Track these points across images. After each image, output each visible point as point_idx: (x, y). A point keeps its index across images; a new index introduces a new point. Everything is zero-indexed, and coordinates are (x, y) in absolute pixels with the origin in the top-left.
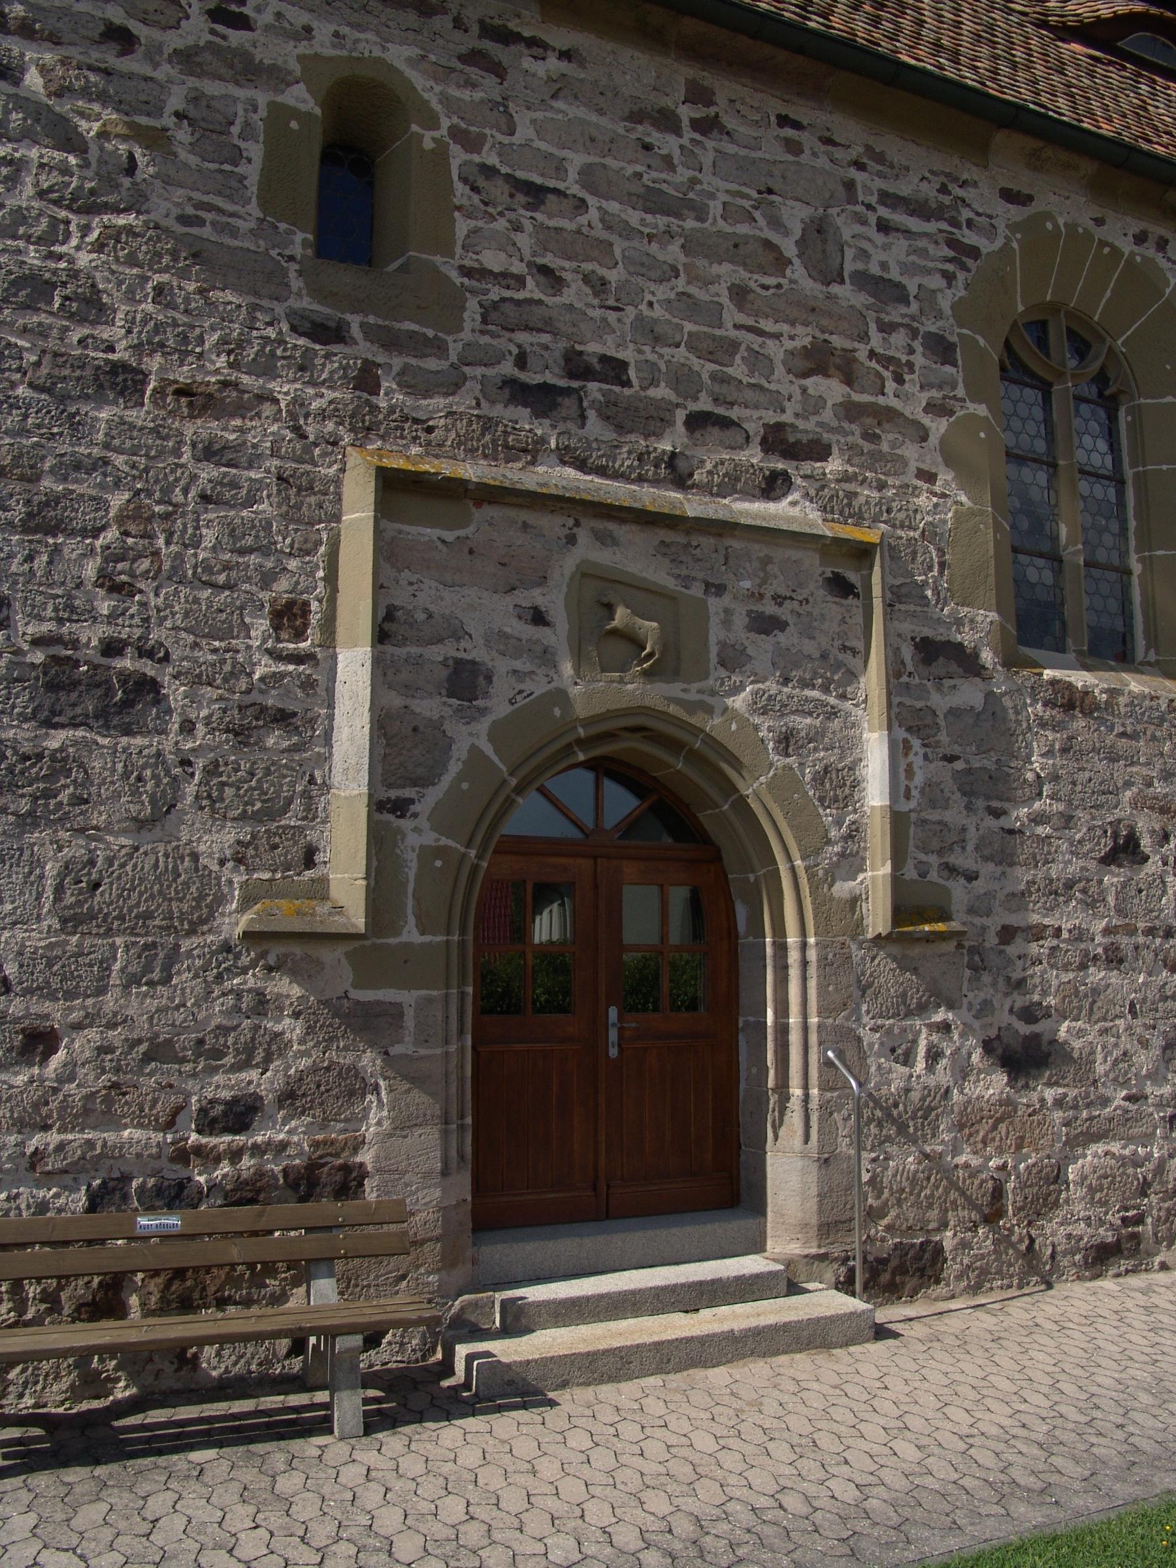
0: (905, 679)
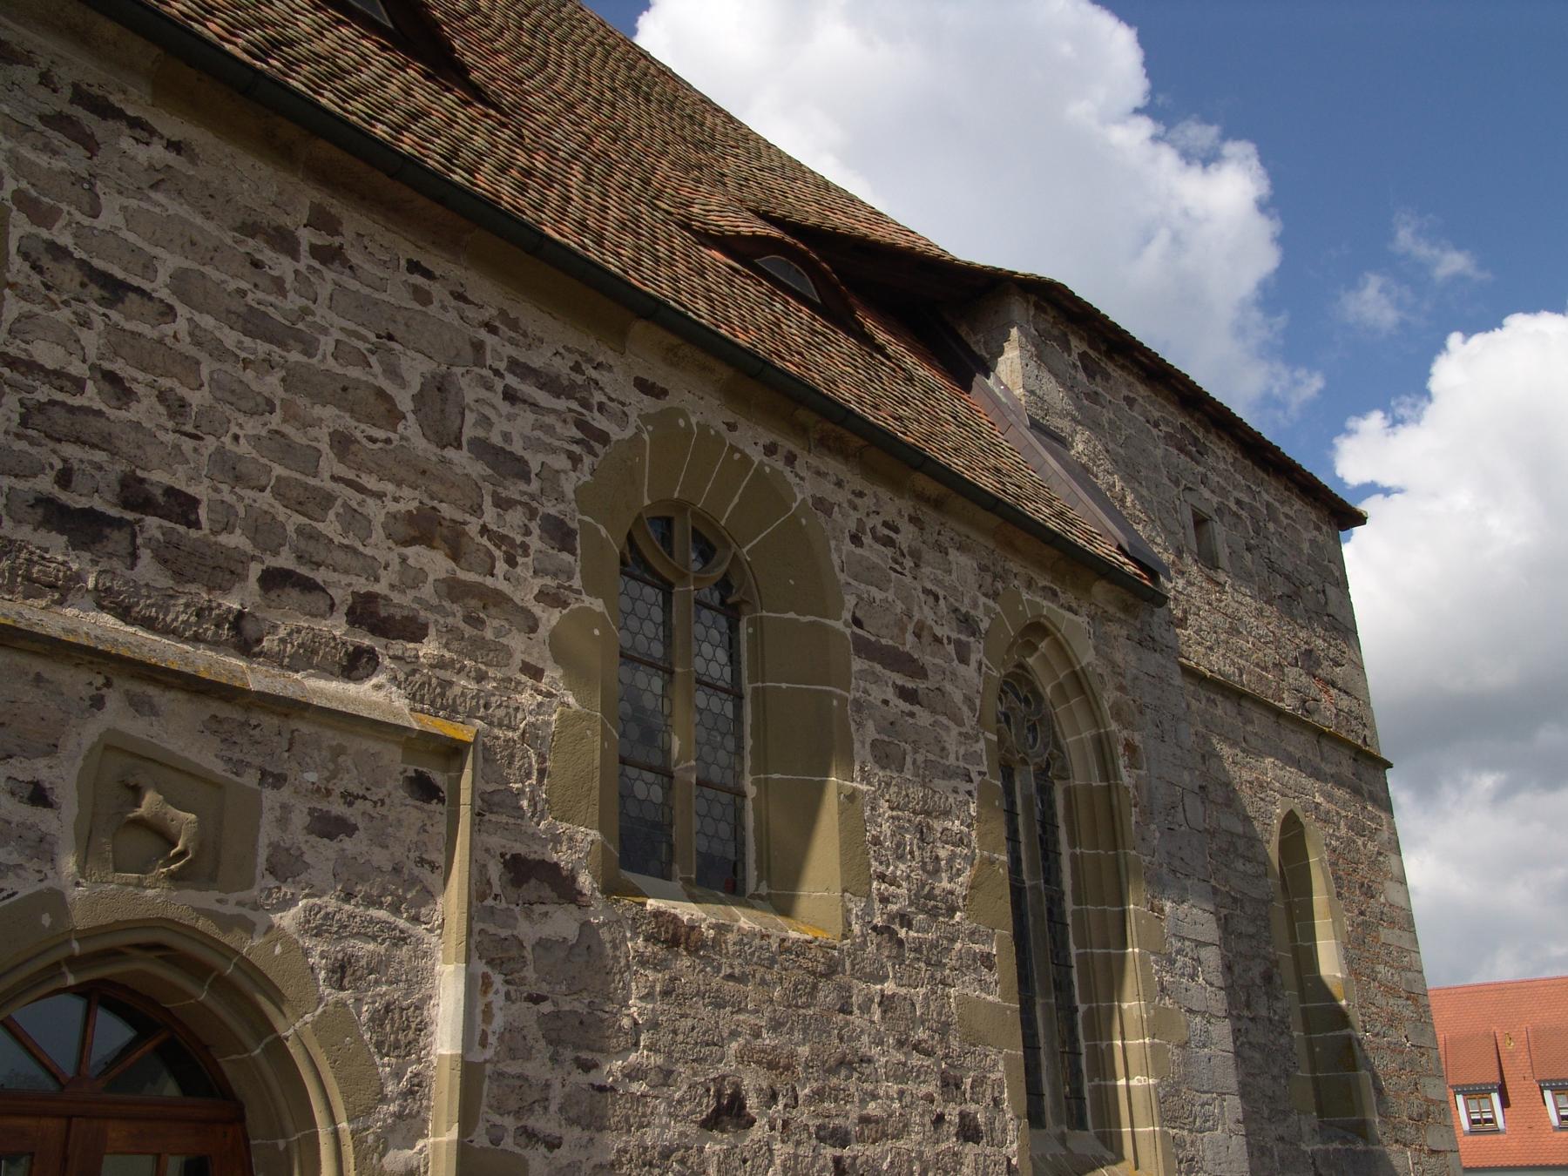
0: (489, 902)
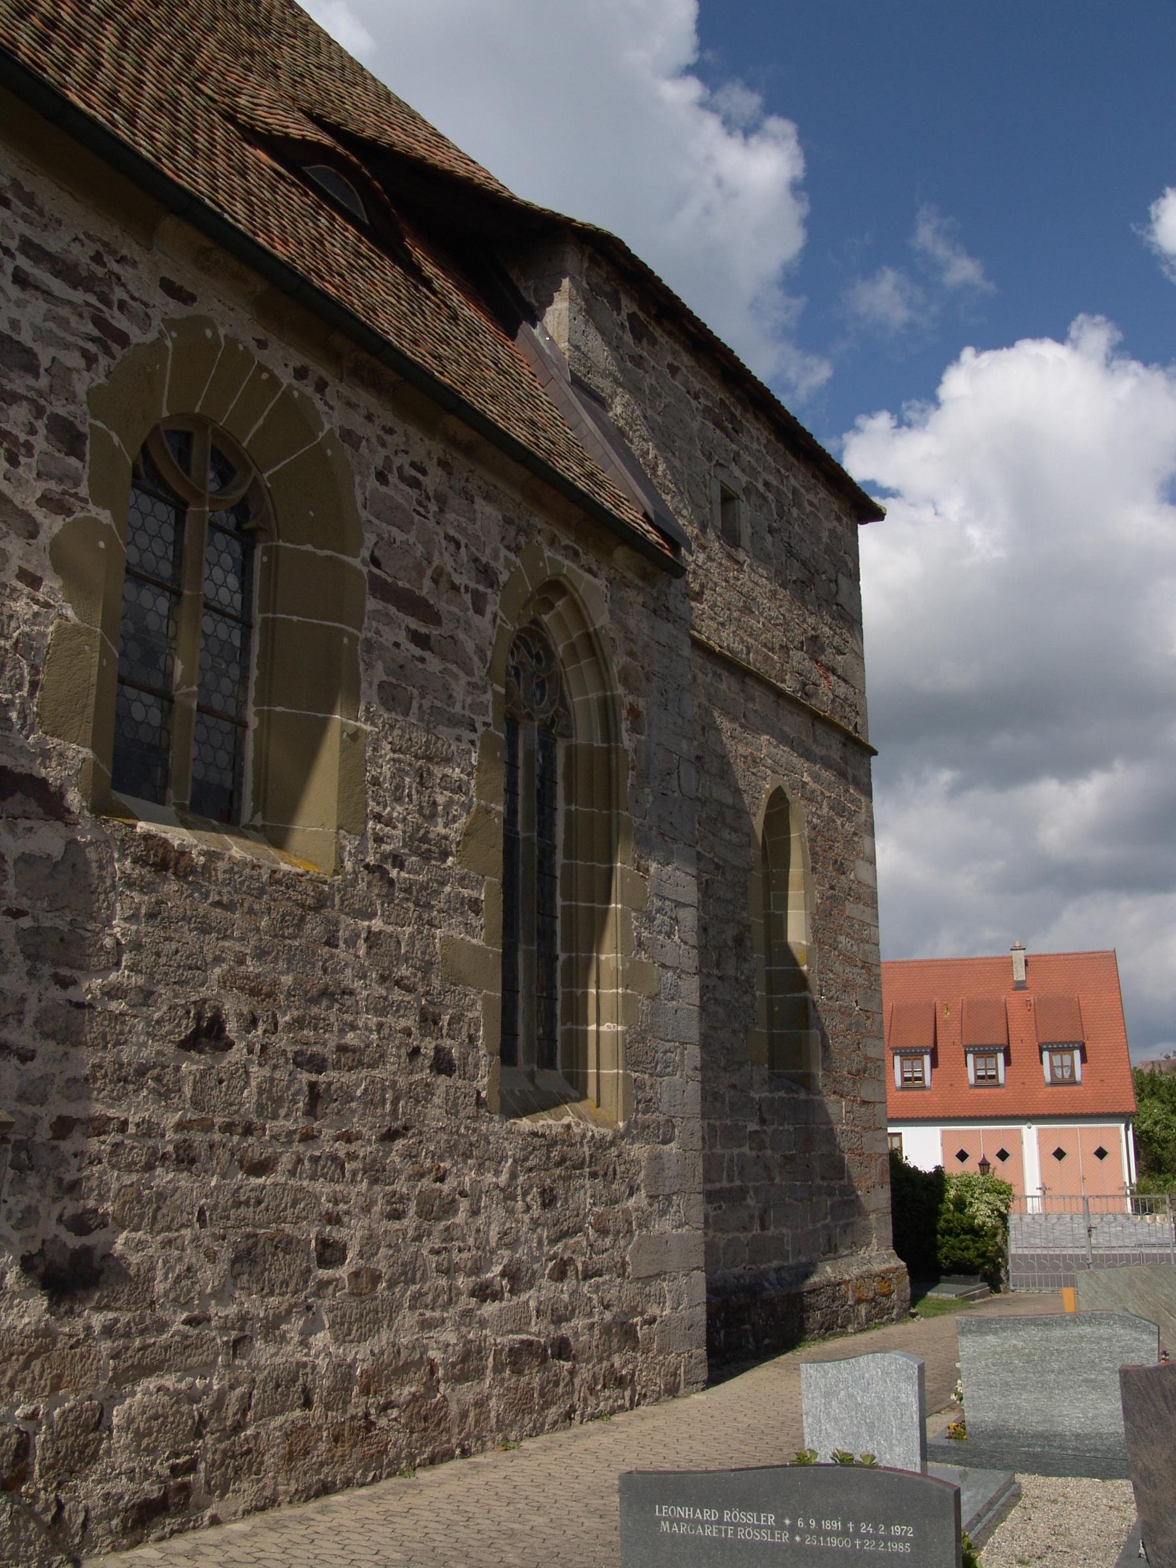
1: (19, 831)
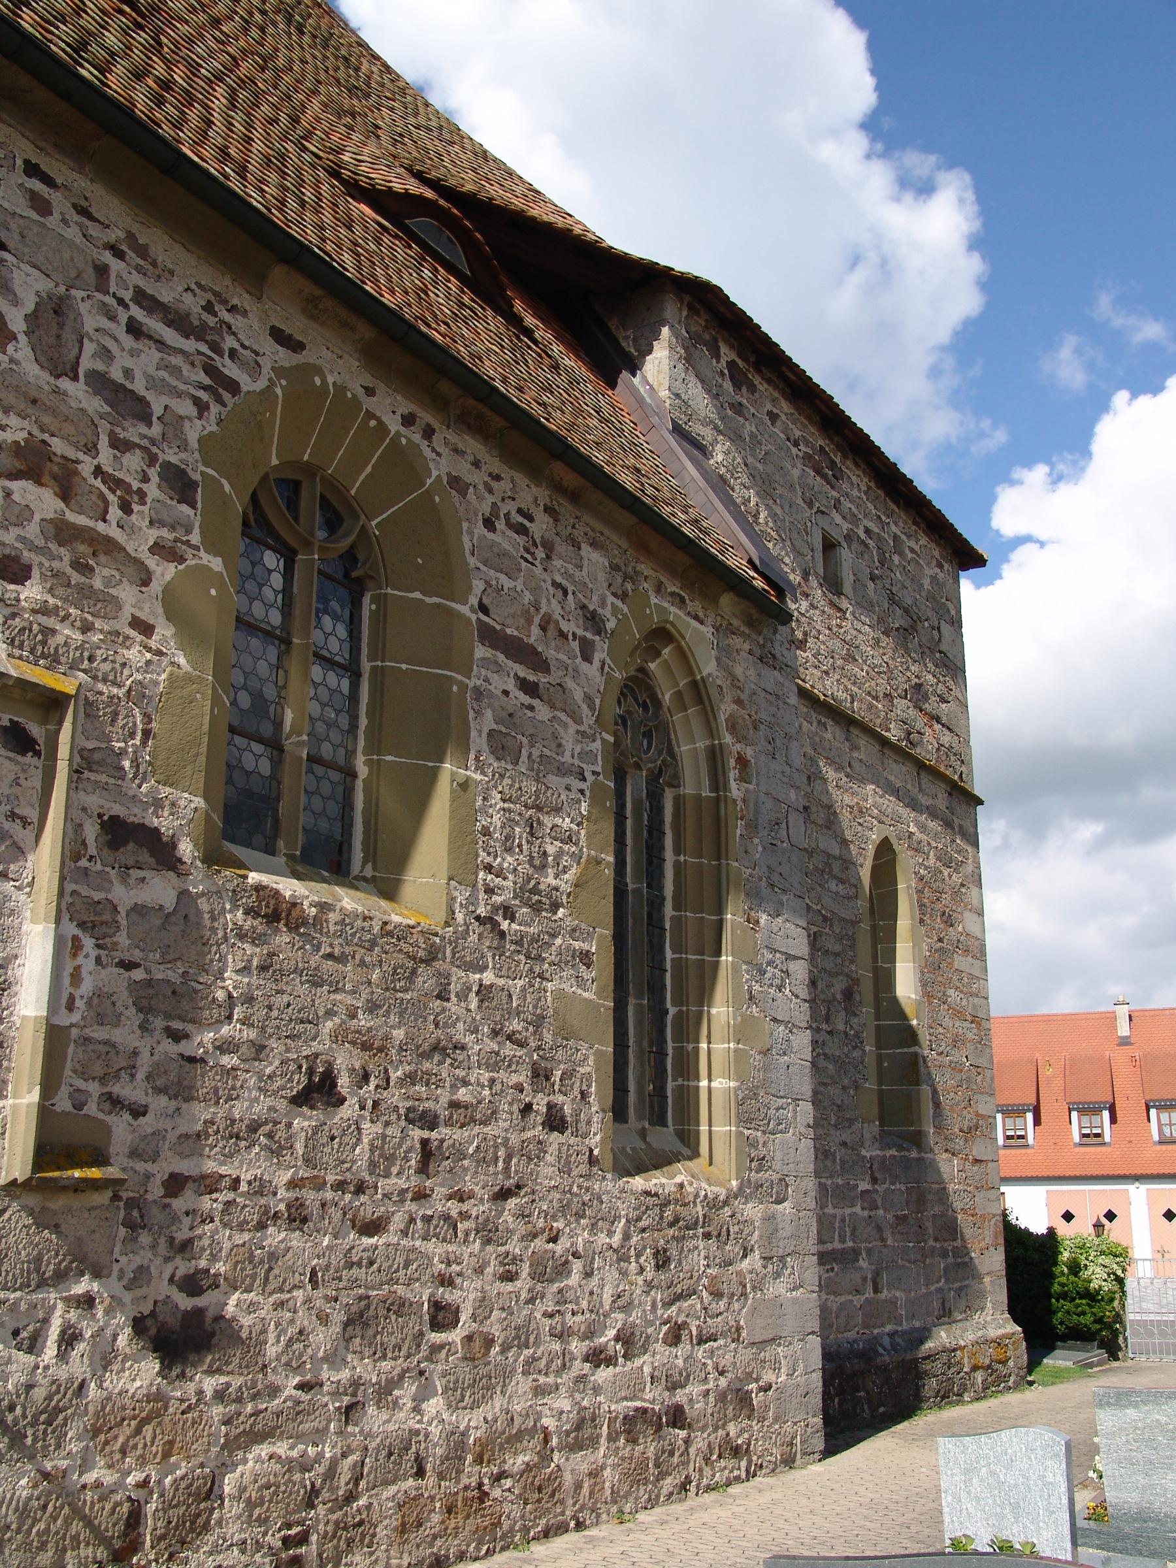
0: (84, 863)
1: (132, 881)
